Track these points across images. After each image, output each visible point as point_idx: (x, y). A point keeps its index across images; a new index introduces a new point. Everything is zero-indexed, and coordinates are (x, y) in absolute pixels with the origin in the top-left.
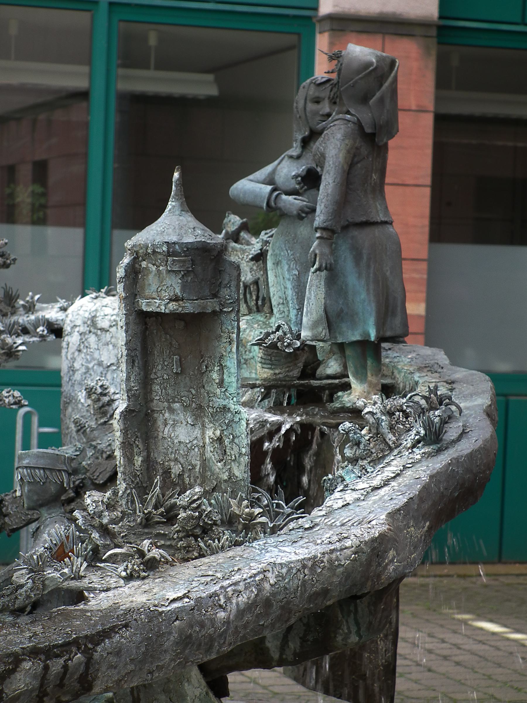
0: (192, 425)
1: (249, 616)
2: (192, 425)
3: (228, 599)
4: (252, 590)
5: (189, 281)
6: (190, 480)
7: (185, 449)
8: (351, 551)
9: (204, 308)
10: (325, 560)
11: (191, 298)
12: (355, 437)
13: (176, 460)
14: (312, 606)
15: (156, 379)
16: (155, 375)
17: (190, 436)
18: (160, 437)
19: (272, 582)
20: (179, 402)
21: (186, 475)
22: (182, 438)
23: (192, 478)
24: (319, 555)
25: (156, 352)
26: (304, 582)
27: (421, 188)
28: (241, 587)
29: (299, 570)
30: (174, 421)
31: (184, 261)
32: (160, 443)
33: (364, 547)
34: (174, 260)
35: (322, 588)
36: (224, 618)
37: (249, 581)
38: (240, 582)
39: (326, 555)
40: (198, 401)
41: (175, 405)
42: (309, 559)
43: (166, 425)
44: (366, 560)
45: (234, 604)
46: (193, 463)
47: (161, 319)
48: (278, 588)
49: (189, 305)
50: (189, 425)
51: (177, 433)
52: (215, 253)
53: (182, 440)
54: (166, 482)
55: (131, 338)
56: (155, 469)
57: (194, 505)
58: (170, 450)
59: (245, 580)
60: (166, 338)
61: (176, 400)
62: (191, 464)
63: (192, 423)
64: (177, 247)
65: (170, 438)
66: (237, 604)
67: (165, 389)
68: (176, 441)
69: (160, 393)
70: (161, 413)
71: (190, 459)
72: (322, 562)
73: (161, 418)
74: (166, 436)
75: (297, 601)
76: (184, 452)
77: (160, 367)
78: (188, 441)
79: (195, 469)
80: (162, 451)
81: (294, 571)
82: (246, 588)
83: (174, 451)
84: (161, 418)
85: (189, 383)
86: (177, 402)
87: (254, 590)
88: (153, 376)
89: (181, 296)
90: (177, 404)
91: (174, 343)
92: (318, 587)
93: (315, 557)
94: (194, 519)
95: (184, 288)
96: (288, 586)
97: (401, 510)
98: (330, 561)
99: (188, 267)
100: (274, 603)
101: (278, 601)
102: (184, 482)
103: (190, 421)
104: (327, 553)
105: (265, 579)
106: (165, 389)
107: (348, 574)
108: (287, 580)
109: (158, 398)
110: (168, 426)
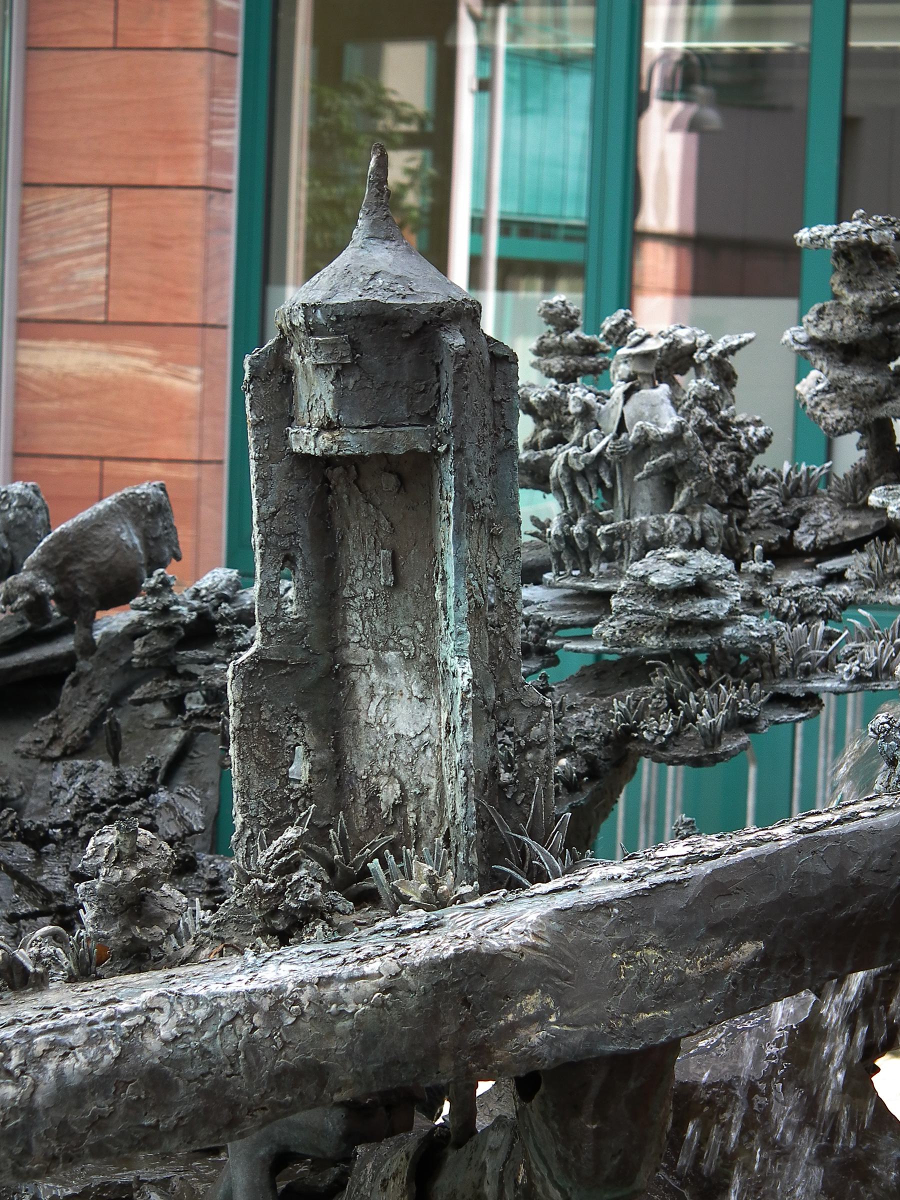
0: (421, 700)
1: (101, 1102)
2: (421, 700)
3: (33, 1061)
4: (107, 1047)
5: (350, 387)
6: (418, 819)
7: (410, 750)
8: (375, 985)
9: (385, 444)
10: (304, 998)
11: (357, 424)
12: (885, 746)
13: (392, 773)
14: (288, 1098)
15: (353, 598)
16: (352, 589)
17: (416, 723)
18: (362, 723)
19: (164, 1033)
20: (396, 650)
21: (411, 807)
22: (403, 727)
23: (422, 814)
24: (290, 986)
25: (351, 542)
26: (252, 1044)
27: (834, 161)
28: (77, 1037)
29: (237, 1015)
30: (387, 689)
31: (334, 345)
32: (362, 737)
33: (409, 978)
34: (317, 343)
35: (304, 1062)
36: (14, 1099)
37: (102, 1025)
38: (77, 1026)
39: (308, 987)
40: (430, 647)
41: (387, 655)
42: (265, 993)
43: (372, 697)
44: (419, 1008)
45: (50, 1073)
46: (423, 781)
47: (357, 469)
48: (185, 1049)
49: (350, 438)
50: (414, 699)
51: (392, 716)
52: (412, 327)
53: (402, 732)
54: (373, 821)
55: (273, 509)
56: (353, 791)
57: (113, 858)
58: (381, 750)
59: (92, 1023)
60: (367, 511)
61: (391, 644)
62: (419, 784)
63: (420, 696)
64: (319, 314)
65: (380, 724)
66: (60, 1074)
67: (370, 621)
68: (391, 732)
69: (360, 628)
70: (364, 671)
71: (418, 772)
72: (297, 1002)
73: (364, 682)
74: (372, 721)
75: (242, 1083)
76: (407, 757)
77: (359, 574)
78: (412, 735)
79: (427, 794)
80: (366, 752)
81: (226, 1016)
82: (90, 1041)
83: (387, 753)
84: (364, 682)
85: (412, 609)
86: (392, 649)
87: (111, 1047)
88: (346, 593)
89: (335, 420)
90: (392, 653)
91: (382, 522)
92: (292, 1058)
93: (281, 990)
94: (265, 896)
95: (340, 398)
96: (211, 1049)
97: (614, 906)
98: (318, 1002)
99: (342, 358)
100: (181, 1082)
101: (192, 1078)
102: (406, 823)
103: (415, 689)
104: (311, 984)
105: (148, 1025)
106: (370, 621)
107: (368, 1035)
108: (207, 1035)
109: (356, 638)
110: (377, 700)
